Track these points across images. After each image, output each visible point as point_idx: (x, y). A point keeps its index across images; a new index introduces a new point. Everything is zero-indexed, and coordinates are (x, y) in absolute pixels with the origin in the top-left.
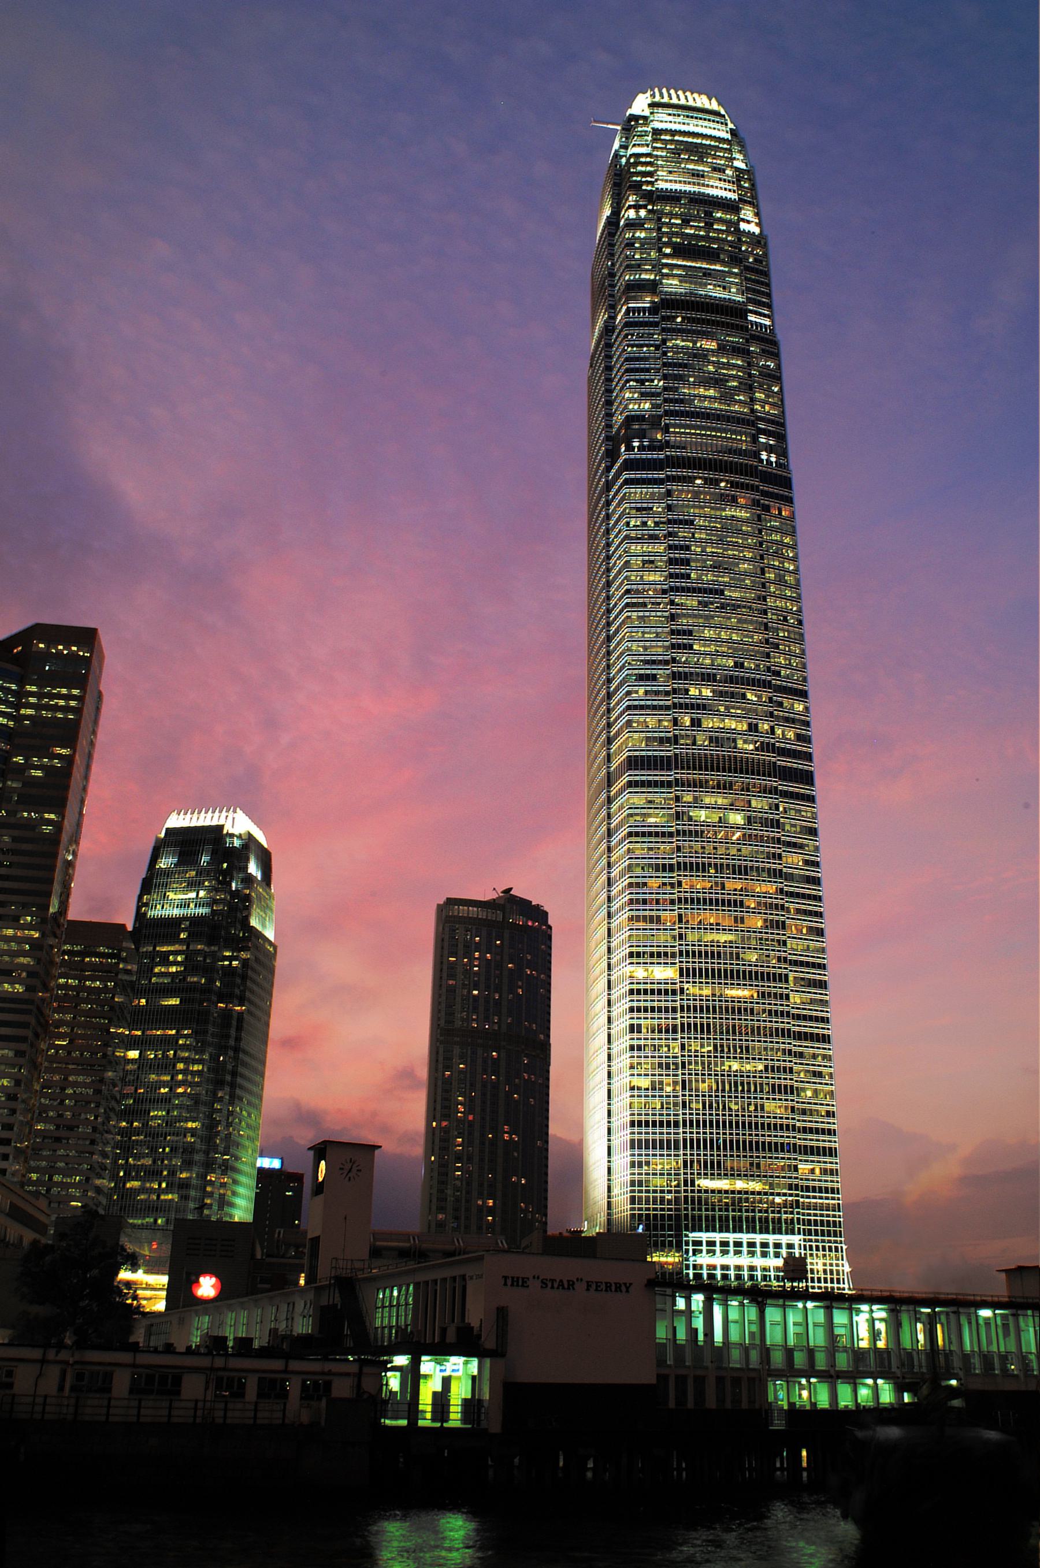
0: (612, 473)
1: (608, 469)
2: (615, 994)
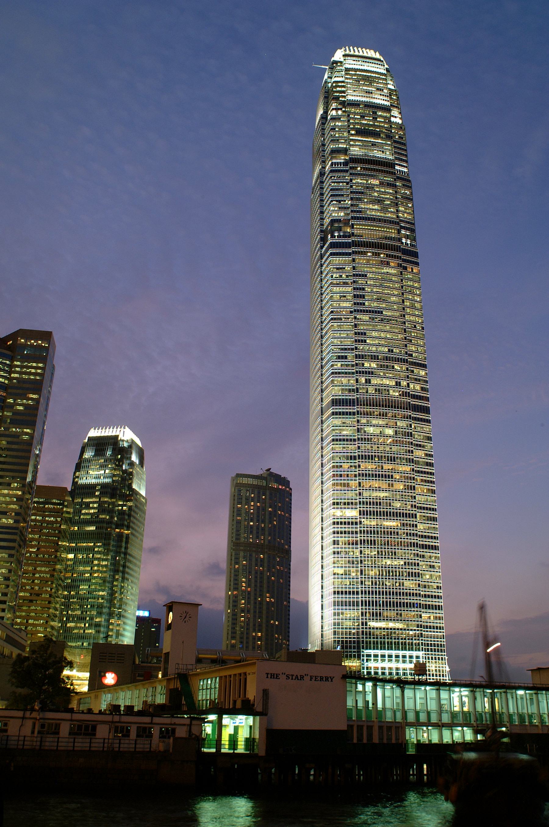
0: (323, 250)
1: (322, 247)
2: (325, 524)
